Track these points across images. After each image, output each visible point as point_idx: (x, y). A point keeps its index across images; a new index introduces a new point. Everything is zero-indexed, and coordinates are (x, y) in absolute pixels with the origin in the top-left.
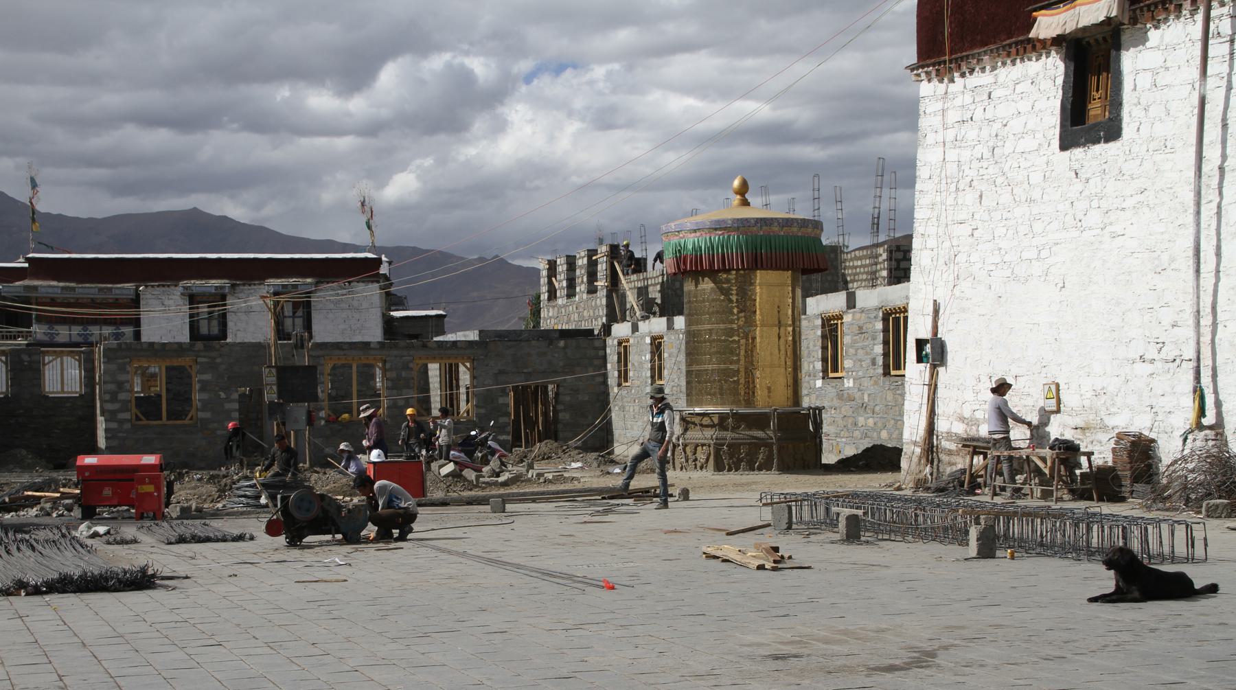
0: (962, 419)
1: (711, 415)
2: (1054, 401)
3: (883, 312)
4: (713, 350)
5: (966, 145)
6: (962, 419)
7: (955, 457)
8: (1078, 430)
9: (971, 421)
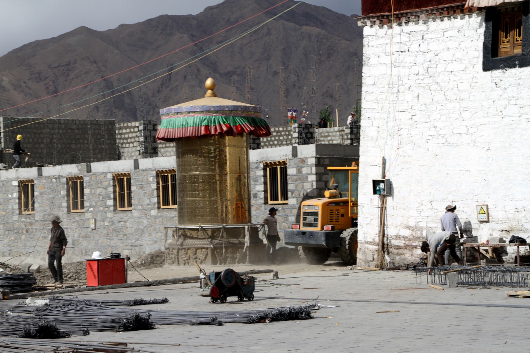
0: (408, 228)
1: (206, 229)
2: (486, 215)
3: (263, 164)
4: (200, 188)
5: (404, 65)
6: (408, 228)
7: (403, 250)
8: (504, 232)
9: (416, 228)
